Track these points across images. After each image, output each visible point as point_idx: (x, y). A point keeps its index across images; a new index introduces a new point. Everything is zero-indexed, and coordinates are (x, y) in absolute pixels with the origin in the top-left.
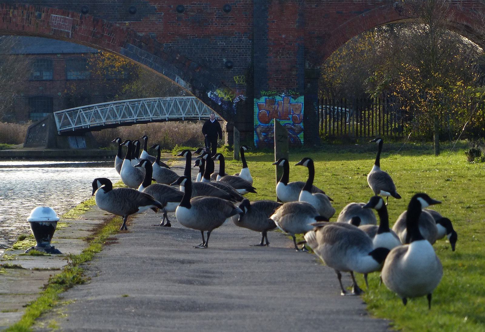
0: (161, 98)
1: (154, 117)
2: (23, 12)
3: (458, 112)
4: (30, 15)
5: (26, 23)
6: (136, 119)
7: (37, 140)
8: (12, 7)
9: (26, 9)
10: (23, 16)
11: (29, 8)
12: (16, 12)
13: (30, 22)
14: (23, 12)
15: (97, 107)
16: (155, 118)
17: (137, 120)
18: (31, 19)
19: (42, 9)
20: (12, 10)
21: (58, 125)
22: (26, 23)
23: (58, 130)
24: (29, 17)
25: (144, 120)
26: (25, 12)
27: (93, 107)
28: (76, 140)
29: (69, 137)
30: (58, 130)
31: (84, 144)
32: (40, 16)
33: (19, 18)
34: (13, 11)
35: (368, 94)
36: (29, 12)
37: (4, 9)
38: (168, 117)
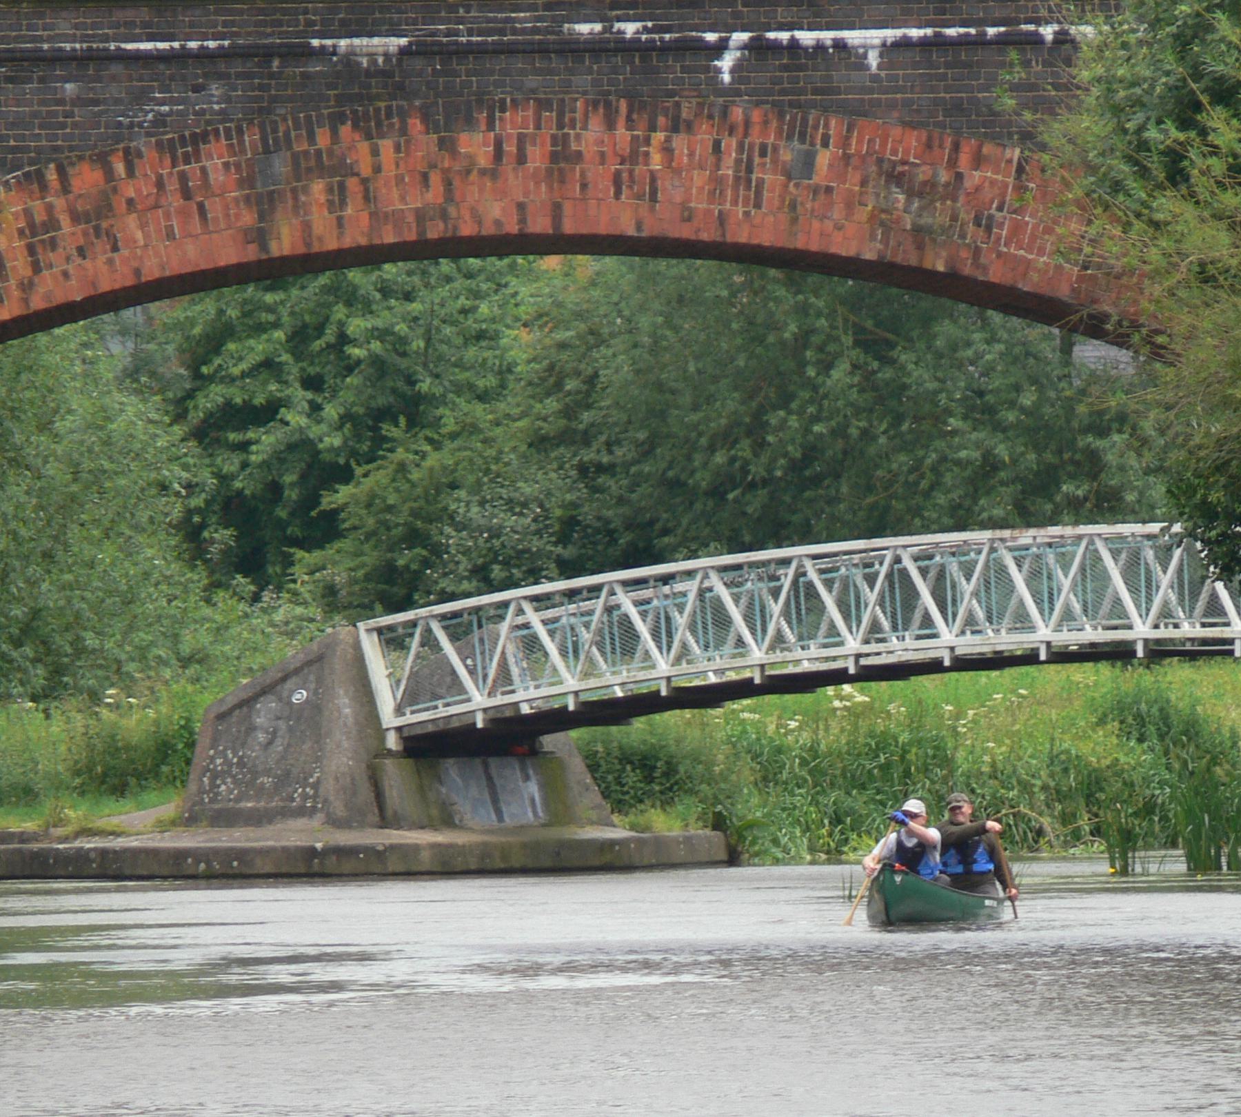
0: (1006, 533)
1: (962, 640)
2: (717, 145)
3: (376, 61)
4: (757, 160)
5: (735, 202)
6: (858, 656)
7: (267, 781)
8: (661, 120)
9: (731, 131)
10: (717, 167)
11: (747, 123)
12: (680, 143)
13: (758, 193)
14: (717, 145)
15: (527, 606)
16: (970, 645)
17: (863, 662)
18: (760, 183)
19: (816, 127)
20: (659, 136)
21: (386, 702)
22: (735, 202)
23: (385, 726)
24: (749, 170)
25: (798, 670)
26: (730, 144)
27: (505, 605)
28: (489, 778)
29: (451, 761)
30: (385, 726)
31: (533, 800)
32: (808, 162)
33: (699, 178)
34: (668, 140)
35: (45, 679)
36: (751, 146)
37: (621, 132)
38: (952, 649)
